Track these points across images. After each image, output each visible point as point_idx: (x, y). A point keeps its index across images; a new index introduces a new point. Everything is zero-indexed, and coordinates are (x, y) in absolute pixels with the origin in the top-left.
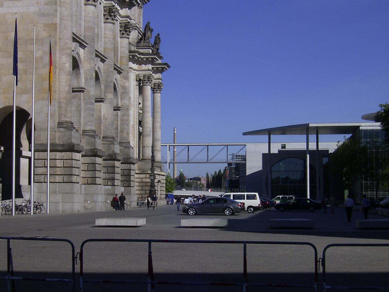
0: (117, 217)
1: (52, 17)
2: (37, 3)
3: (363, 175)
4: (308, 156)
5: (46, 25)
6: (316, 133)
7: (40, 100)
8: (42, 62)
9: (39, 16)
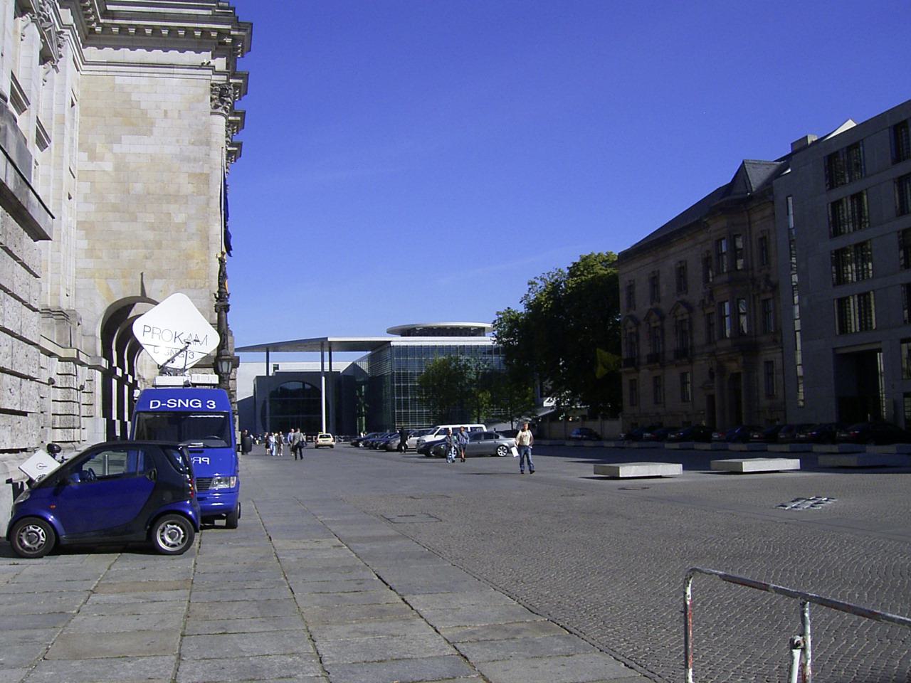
0: (629, 462)
1: (201, 163)
2: (178, 141)
3: (801, 403)
4: (323, 378)
5: (192, 176)
6: (328, 349)
7: (183, 288)
8: (185, 231)
9: (181, 161)
